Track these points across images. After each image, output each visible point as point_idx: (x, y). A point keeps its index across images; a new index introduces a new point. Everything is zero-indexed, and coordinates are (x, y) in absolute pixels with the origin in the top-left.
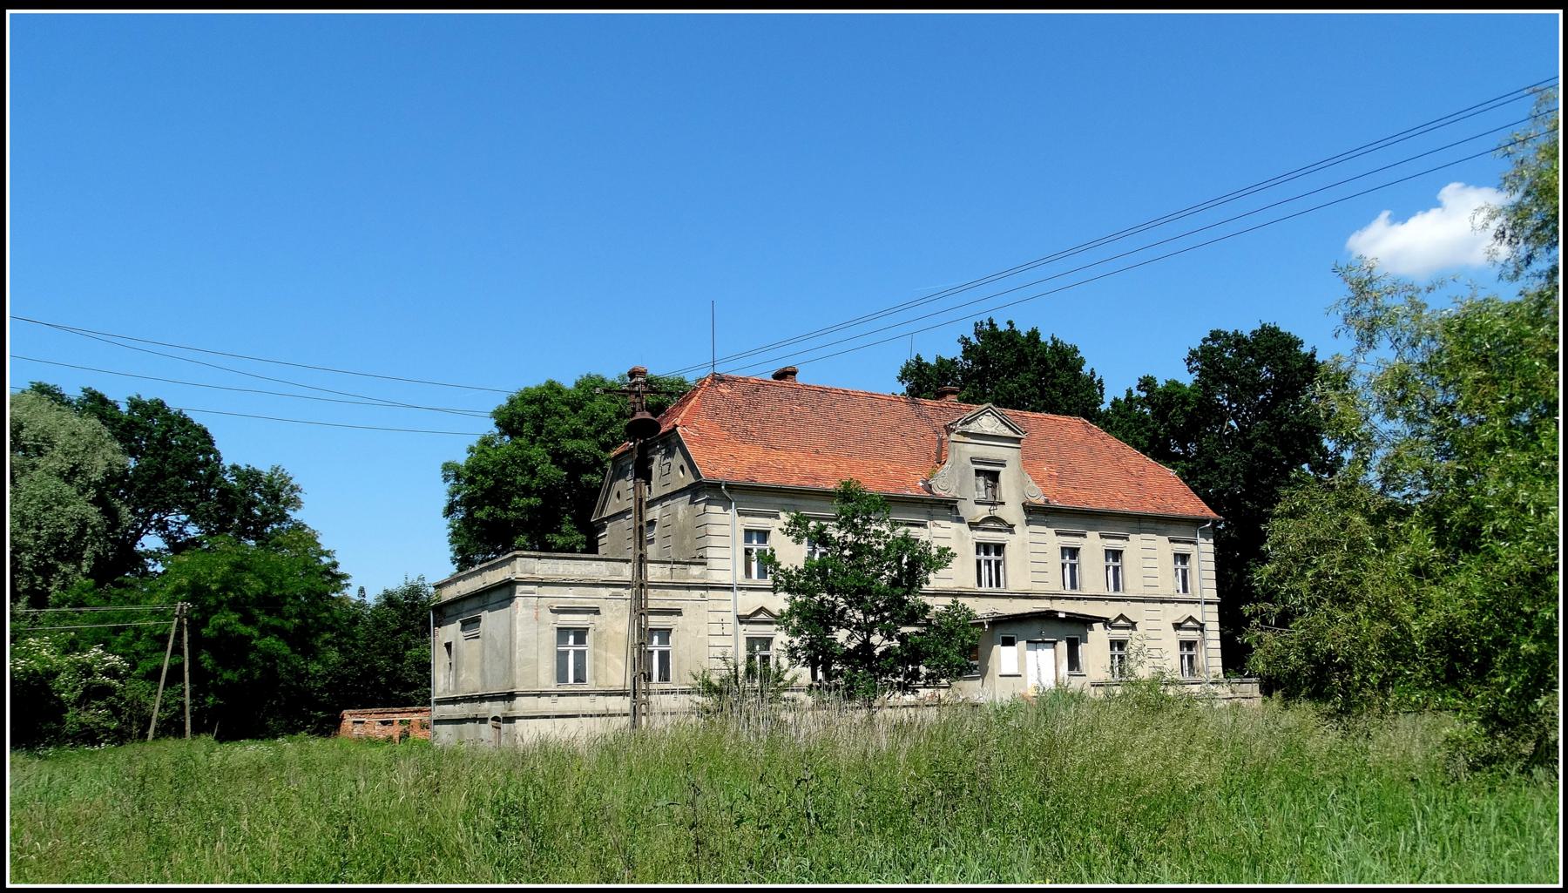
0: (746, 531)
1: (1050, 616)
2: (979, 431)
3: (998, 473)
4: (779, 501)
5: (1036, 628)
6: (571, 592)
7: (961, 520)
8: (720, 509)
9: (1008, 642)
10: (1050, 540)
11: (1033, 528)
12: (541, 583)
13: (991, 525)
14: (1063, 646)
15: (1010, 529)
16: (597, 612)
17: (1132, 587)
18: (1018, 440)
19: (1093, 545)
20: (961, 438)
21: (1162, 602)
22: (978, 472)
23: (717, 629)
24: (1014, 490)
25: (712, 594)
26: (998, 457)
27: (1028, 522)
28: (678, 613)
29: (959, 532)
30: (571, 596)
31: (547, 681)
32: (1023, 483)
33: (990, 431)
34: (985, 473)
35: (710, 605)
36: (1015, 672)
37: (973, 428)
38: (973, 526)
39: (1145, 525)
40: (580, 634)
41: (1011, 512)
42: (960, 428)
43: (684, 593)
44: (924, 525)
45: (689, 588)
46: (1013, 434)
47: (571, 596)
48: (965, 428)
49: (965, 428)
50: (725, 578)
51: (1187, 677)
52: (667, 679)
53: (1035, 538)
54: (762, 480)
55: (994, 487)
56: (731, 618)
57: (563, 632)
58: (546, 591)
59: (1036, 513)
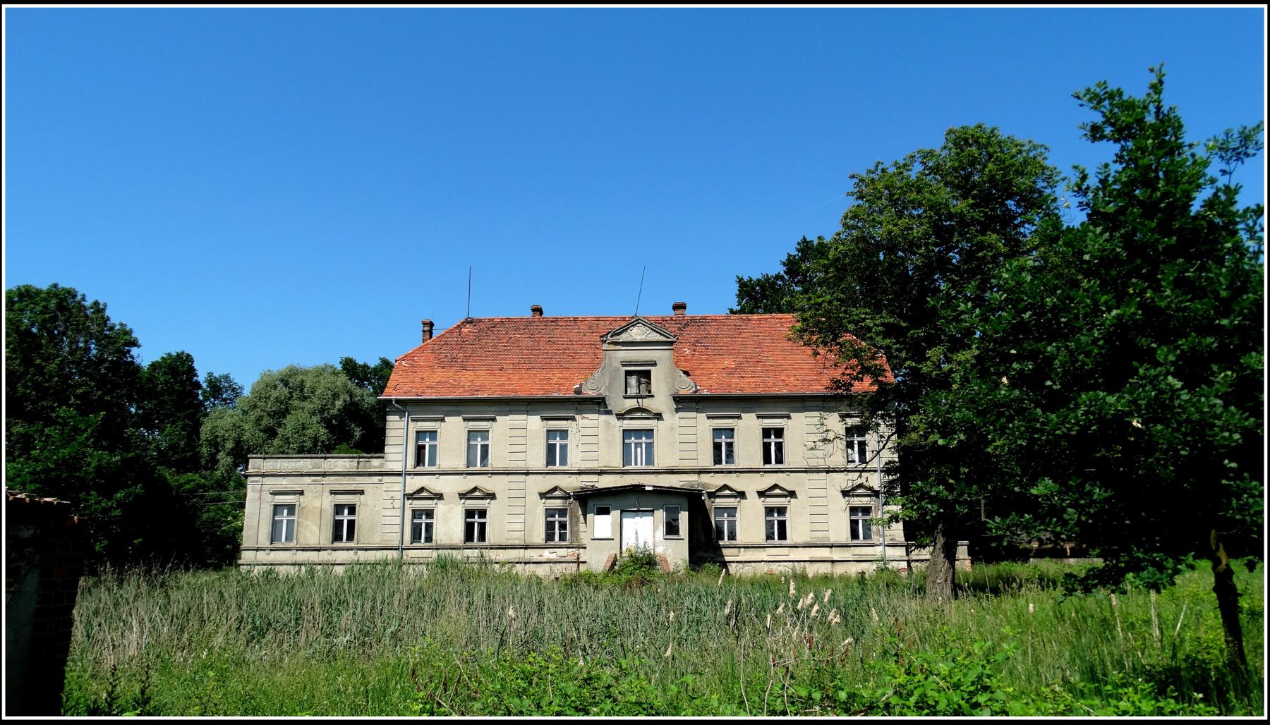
0: (733, 430)
1: (637, 490)
2: (630, 339)
3: (649, 372)
4: (445, 409)
5: (632, 499)
6: (284, 481)
7: (609, 413)
8: (397, 418)
9: (604, 511)
10: (703, 424)
11: (681, 414)
12: (263, 475)
13: (639, 415)
14: (661, 515)
15: (659, 416)
16: (302, 493)
17: (495, 461)
18: (671, 343)
19: (748, 428)
20: (613, 347)
21: (828, 472)
22: (628, 373)
23: (388, 504)
24: (663, 386)
25: (386, 479)
26: (649, 359)
27: (677, 410)
28: (362, 492)
29: (607, 423)
30: (284, 483)
31: (264, 541)
32: (674, 379)
33: (639, 339)
34: (639, 373)
35: (384, 487)
36: (609, 536)
37: (624, 337)
38: (620, 417)
39: (808, 404)
40: (291, 509)
41: (660, 400)
42: (611, 340)
43: (367, 479)
44: (573, 419)
45: (370, 475)
46: (663, 339)
47: (284, 483)
48: (615, 339)
49: (615, 339)
50: (398, 467)
51: (776, 541)
52: (785, 538)
53: (683, 422)
54: (774, 391)
55: (649, 383)
56: (400, 495)
57: (277, 508)
58: (267, 480)
59: (683, 403)
